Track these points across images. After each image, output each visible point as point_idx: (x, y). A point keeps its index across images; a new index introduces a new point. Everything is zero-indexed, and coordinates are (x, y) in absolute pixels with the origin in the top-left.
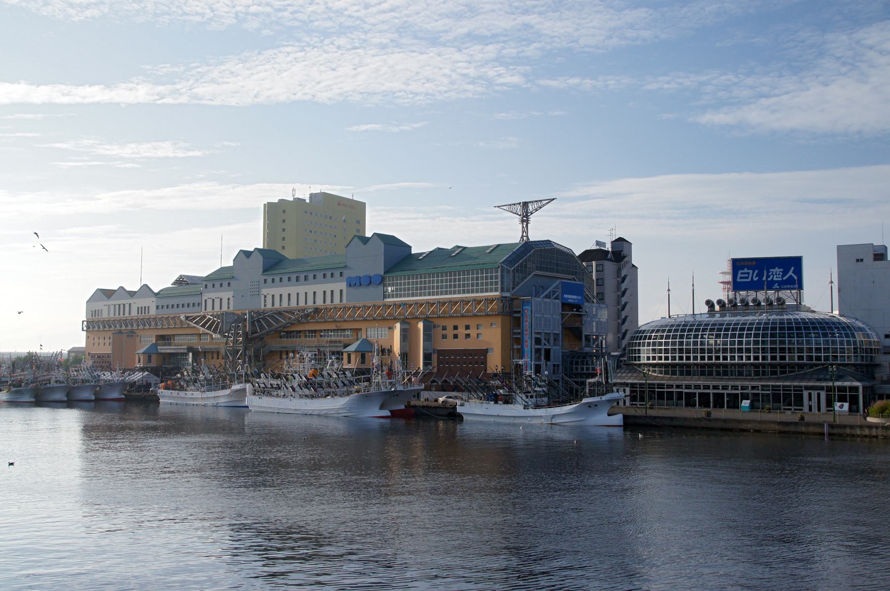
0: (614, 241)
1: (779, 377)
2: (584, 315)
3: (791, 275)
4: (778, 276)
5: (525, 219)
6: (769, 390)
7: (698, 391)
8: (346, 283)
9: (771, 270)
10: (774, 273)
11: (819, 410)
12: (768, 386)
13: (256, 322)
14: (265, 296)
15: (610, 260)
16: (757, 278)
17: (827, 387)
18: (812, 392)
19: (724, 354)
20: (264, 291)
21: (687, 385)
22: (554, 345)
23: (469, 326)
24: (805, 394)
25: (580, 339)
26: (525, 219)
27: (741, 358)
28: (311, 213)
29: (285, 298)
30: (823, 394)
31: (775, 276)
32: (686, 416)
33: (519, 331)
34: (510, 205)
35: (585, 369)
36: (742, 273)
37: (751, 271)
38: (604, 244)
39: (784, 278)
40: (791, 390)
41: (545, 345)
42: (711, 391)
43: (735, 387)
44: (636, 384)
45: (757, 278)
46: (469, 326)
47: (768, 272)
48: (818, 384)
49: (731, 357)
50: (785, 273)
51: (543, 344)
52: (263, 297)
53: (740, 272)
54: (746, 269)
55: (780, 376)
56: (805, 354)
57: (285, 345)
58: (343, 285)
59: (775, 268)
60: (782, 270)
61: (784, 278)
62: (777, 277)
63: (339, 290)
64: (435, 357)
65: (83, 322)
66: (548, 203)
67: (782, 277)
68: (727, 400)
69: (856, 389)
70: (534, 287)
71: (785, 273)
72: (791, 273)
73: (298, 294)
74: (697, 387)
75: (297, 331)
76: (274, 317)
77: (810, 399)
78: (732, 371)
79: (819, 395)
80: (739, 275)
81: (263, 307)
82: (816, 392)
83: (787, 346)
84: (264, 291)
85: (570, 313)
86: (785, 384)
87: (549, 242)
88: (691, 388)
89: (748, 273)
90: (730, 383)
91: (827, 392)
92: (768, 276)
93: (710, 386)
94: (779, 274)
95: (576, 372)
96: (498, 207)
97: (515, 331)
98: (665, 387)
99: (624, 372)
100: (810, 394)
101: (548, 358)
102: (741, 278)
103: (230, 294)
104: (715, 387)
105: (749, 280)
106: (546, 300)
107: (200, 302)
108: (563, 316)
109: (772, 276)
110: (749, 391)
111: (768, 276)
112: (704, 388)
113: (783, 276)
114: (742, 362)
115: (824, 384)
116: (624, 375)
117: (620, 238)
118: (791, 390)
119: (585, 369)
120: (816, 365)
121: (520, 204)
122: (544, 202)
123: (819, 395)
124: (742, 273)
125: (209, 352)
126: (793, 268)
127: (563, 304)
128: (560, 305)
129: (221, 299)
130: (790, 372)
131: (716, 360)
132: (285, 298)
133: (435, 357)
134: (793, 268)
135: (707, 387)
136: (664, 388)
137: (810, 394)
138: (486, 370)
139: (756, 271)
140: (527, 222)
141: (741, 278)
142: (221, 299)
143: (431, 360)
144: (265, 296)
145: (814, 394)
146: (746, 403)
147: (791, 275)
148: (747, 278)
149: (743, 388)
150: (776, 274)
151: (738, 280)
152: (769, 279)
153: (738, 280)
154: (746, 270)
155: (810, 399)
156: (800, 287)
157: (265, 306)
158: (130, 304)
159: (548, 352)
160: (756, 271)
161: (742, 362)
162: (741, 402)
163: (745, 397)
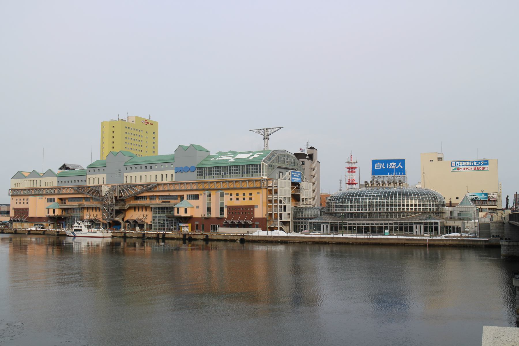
0: (308, 149)
1: (402, 219)
2: (301, 188)
3: (400, 167)
4: (394, 166)
5: (266, 138)
6: (398, 225)
7: (363, 226)
8: (100, 159)
9: (390, 164)
10: (392, 165)
11: (420, 232)
12: (397, 223)
13: (121, 191)
14: (126, 177)
15: (307, 159)
16: (385, 167)
17: (424, 223)
18: (417, 225)
19: (391, 208)
20: (125, 174)
21: (358, 223)
22: (288, 204)
23: (238, 194)
24: (414, 226)
25: (299, 201)
26: (266, 138)
27: (366, 209)
28: (129, 128)
29: (134, 178)
30: (422, 226)
31: (392, 166)
32: (340, 241)
33: (271, 196)
34: (258, 130)
35: (301, 215)
36: (377, 165)
37: (381, 164)
38: (303, 151)
39: (396, 168)
40: (402, 225)
41: (284, 203)
42: (369, 226)
43: (381, 224)
44: (333, 223)
45: (385, 167)
46: (238, 194)
47: (389, 164)
48: (420, 221)
49: (361, 209)
50: (397, 166)
51: (283, 203)
52: (125, 178)
53: (376, 164)
54: (379, 163)
55: (403, 218)
56: (410, 208)
57: (138, 204)
58: (173, 172)
59: (392, 163)
60: (396, 163)
61: (396, 168)
62: (393, 167)
63: (64, 164)
64: (226, 210)
65: (9, 190)
66: (280, 129)
67: (396, 167)
68: (378, 230)
69: (437, 223)
70: (277, 174)
71: (397, 166)
72: (399, 165)
73: (141, 176)
74: (363, 224)
75: (143, 196)
76: (132, 188)
77: (416, 228)
78: (361, 216)
79: (420, 227)
80: (376, 166)
81: (125, 183)
82: (419, 225)
83: (393, 204)
84: (125, 174)
85: (296, 187)
86: (405, 221)
87: (284, 151)
88: (360, 224)
89: (380, 165)
90: (361, 222)
91: (424, 225)
92: (389, 166)
93: (351, 223)
94: (394, 166)
95: (299, 217)
96: (252, 130)
97: (268, 196)
98: (348, 224)
99: (326, 217)
100: (416, 226)
101: (285, 210)
102: (377, 167)
103: (105, 176)
104: (372, 224)
105: (380, 168)
106: (284, 180)
107: (85, 179)
108: (292, 189)
109: (391, 166)
110: (389, 225)
111: (389, 166)
112: (367, 224)
113: (396, 166)
114: (370, 211)
115: (423, 221)
116: (326, 218)
117: (312, 147)
118: (402, 225)
119: (301, 215)
120: (418, 213)
121: (263, 129)
122: (277, 129)
123: (420, 227)
124: (377, 165)
125: (90, 207)
126: (400, 163)
127: (292, 182)
128: (291, 182)
129: (99, 178)
130: (407, 216)
131: (361, 210)
132: (134, 178)
133: (226, 210)
134: (400, 163)
135: (368, 224)
136: (347, 225)
137: (416, 226)
138: (254, 217)
139: (384, 164)
140: (268, 138)
141: (377, 167)
142: (99, 178)
143: (224, 211)
144: (126, 177)
145: (418, 226)
146: (387, 231)
147: (400, 167)
148: (379, 167)
149: (385, 224)
150: (393, 165)
151: (375, 168)
152: (389, 168)
153: (375, 168)
154: (379, 164)
155: (416, 228)
156: (404, 174)
157: (126, 182)
158: (36, 180)
159: (285, 207)
160: (384, 164)
161: (370, 211)
162: (385, 230)
163: (386, 228)
